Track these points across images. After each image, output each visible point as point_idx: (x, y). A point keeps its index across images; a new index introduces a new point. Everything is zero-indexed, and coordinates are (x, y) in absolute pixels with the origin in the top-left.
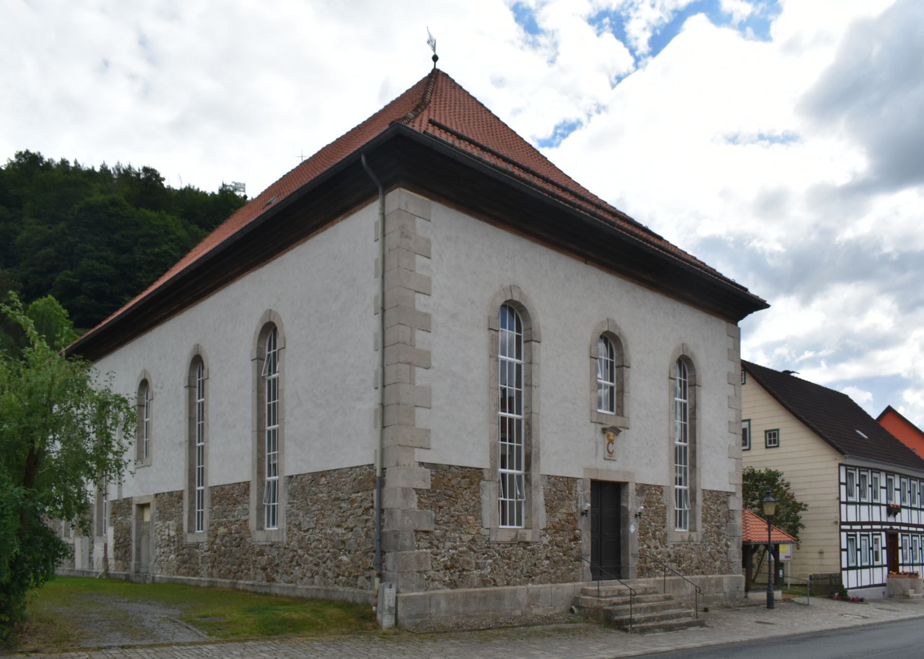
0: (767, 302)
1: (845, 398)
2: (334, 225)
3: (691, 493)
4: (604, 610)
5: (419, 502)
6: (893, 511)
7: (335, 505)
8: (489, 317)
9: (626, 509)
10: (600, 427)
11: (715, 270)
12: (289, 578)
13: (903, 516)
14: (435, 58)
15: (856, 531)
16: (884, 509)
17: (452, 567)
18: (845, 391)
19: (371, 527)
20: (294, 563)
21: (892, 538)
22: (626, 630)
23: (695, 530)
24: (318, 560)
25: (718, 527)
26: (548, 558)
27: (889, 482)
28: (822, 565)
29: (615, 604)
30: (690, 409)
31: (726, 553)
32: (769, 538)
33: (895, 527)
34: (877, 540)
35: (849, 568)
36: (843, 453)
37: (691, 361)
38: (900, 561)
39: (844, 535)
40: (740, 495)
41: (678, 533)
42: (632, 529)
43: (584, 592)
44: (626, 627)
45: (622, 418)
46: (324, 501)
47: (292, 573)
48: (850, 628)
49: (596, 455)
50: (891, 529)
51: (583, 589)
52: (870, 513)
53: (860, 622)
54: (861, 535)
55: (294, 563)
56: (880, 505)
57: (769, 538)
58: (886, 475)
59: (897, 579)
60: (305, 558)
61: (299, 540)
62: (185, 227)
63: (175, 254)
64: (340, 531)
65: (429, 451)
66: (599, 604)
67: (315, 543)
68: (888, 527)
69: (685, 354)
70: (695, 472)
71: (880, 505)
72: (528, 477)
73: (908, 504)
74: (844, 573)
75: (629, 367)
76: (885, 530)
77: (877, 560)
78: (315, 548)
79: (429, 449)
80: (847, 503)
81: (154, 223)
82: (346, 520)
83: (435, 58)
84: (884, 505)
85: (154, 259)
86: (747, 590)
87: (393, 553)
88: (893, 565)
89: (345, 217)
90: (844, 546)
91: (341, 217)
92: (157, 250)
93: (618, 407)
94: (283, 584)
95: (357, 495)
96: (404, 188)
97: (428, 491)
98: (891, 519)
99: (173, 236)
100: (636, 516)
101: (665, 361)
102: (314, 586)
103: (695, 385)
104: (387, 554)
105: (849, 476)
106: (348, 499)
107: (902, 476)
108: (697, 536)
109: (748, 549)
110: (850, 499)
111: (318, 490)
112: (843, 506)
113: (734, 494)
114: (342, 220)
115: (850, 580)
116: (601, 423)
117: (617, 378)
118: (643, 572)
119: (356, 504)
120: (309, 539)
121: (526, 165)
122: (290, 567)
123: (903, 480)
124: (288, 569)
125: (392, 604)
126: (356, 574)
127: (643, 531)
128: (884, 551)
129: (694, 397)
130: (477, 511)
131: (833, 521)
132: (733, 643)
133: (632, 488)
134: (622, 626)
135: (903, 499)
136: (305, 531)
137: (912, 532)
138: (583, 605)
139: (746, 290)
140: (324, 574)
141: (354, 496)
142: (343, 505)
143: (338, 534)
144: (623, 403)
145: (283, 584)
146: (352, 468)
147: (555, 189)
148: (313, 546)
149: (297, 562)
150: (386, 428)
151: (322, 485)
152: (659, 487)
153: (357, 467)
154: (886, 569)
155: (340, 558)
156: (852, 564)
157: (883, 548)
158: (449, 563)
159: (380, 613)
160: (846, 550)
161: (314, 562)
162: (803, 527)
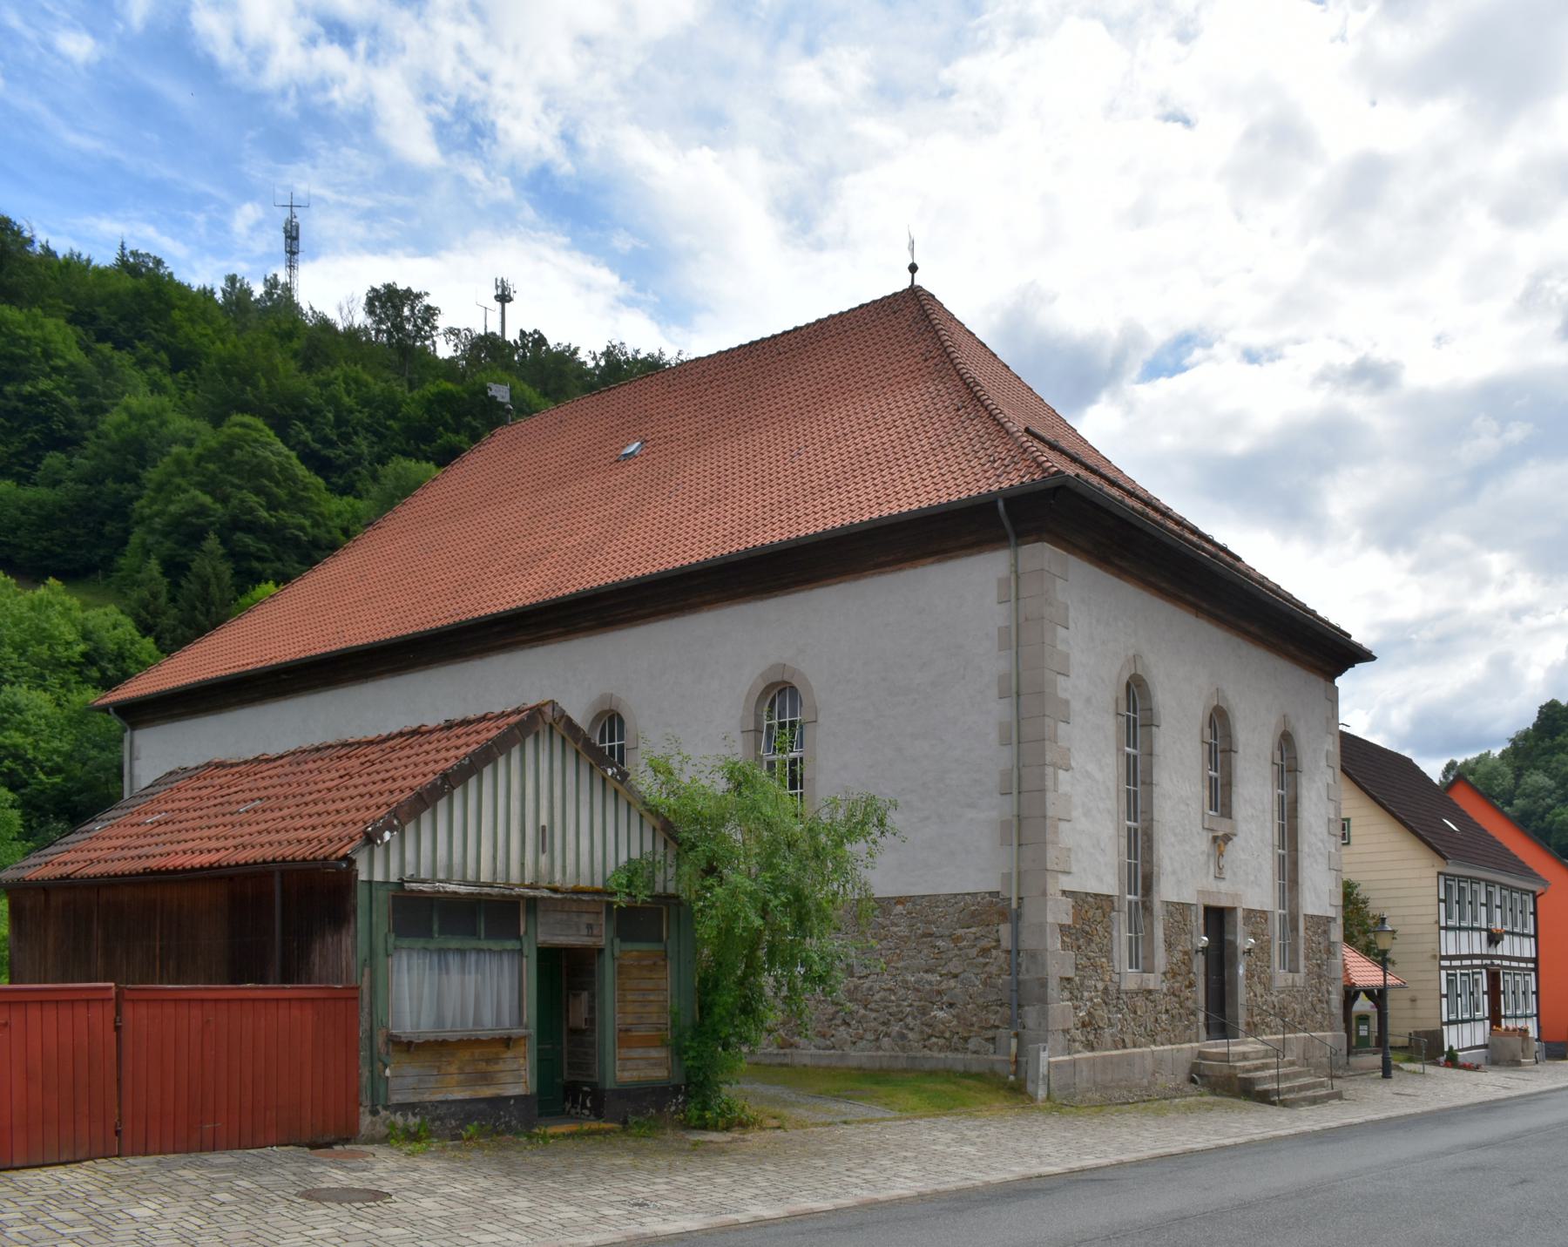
0: (1374, 654)
1: (1408, 762)
2: (916, 567)
3: (1291, 920)
4: (1240, 1078)
5: (1063, 942)
6: (1494, 939)
7: (924, 943)
8: (1117, 699)
9: (1233, 944)
10: (1211, 835)
11: (1279, 587)
12: (828, 1042)
13: (1504, 948)
14: (913, 268)
15: (1455, 968)
16: (1484, 934)
17: (1090, 1023)
18: (1407, 753)
19: (995, 972)
20: (838, 1022)
21: (1494, 978)
22: (1273, 1103)
23: (1297, 971)
24: (887, 1016)
25: (1319, 965)
26: (1167, 1011)
27: (1489, 895)
28: (1414, 1018)
29: (1248, 1071)
30: (1288, 803)
31: (1327, 1002)
32: (1385, 980)
33: (1497, 962)
34: (1477, 980)
35: (1449, 1023)
36: (1444, 858)
37: (1292, 739)
38: (1503, 1013)
39: (1443, 973)
40: (1340, 921)
41: (1282, 977)
42: (1241, 971)
43: (1202, 1055)
44: (1272, 1099)
45: (1229, 821)
46: (901, 937)
47: (833, 1036)
48: (1504, 1100)
49: (1208, 873)
50: (1492, 964)
51: (1200, 1052)
52: (1457, 942)
53: (1503, 1094)
54: (1461, 974)
55: (838, 1022)
56: (1480, 929)
57: (1385, 980)
58: (1487, 886)
59: (1503, 1038)
60: (860, 1014)
61: (848, 991)
62: (88, 350)
63: (66, 399)
64: (935, 978)
65: (1070, 876)
66: (1232, 1071)
67: (882, 993)
68: (1489, 962)
69: (1139, 672)
70: (1297, 890)
71: (1480, 929)
72: (1148, 904)
73: (1508, 928)
74: (1445, 1028)
75: (1236, 752)
76: (1485, 966)
77: (1478, 1011)
78: (883, 1000)
79: (1069, 873)
80: (1447, 928)
81: (20, 331)
82: (946, 964)
83: (913, 268)
84: (1484, 930)
85: (20, 405)
86: (1349, 1053)
87: (1037, 1007)
88: (1495, 1017)
89: (939, 561)
90: (1444, 991)
91: (930, 560)
92: (27, 388)
93: (1223, 805)
94: (813, 1051)
95: (967, 930)
96: (1048, 542)
97: (1069, 926)
98: (1492, 951)
99: (60, 363)
100: (1244, 953)
101: (1198, 713)
102: (881, 1053)
103: (1296, 770)
104: (1026, 1008)
105: (1448, 888)
106: (950, 936)
107: (1503, 886)
108: (1300, 978)
109: (1351, 994)
110: (1450, 923)
111: (888, 922)
112: (1443, 932)
113: (1334, 919)
114: (933, 563)
115: (1453, 1038)
116: (1212, 830)
117: (1222, 767)
118: (1253, 1030)
119: (965, 943)
120: (870, 989)
121: (1072, 451)
122: (830, 1027)
123: (1504, 892)
124: (826, 1029)
125: (1046, 1073)
126: (966, 1035)
127: (1250, 975)
128: (1486, 996)
129: (1295, 786)
130: (1107, 952)
131: (1430, 954)
132: (1007, 1183)
133: (1240, 914)
134: (1264, 1098)
135: (1504, 923)
136: (860, 978)
137: (1522, 969)
138: (1206, 1073)
139: (1350, 636)
140: (903, 1037)
141: (960, 932)
142: (940, 943)
143: (930, 983)
144: (1230, 801)
145: (813, 1051)
146: (955, 895)
147: (1102, 482)
148: (877, 997)
149: (844, 1020)
150: (1024, 847)
151: (896, 915)
152: (1264, 912)
153: (968, 894)
154: (1487, 1022)
155: (932, 1014)
156: (1453, 1017)
157: (1484, 993)
158: (1087, 1018)
159: (1033, 1082)
160: (1446, 996)
161: (882, 1020)
162: (1393, 963)
